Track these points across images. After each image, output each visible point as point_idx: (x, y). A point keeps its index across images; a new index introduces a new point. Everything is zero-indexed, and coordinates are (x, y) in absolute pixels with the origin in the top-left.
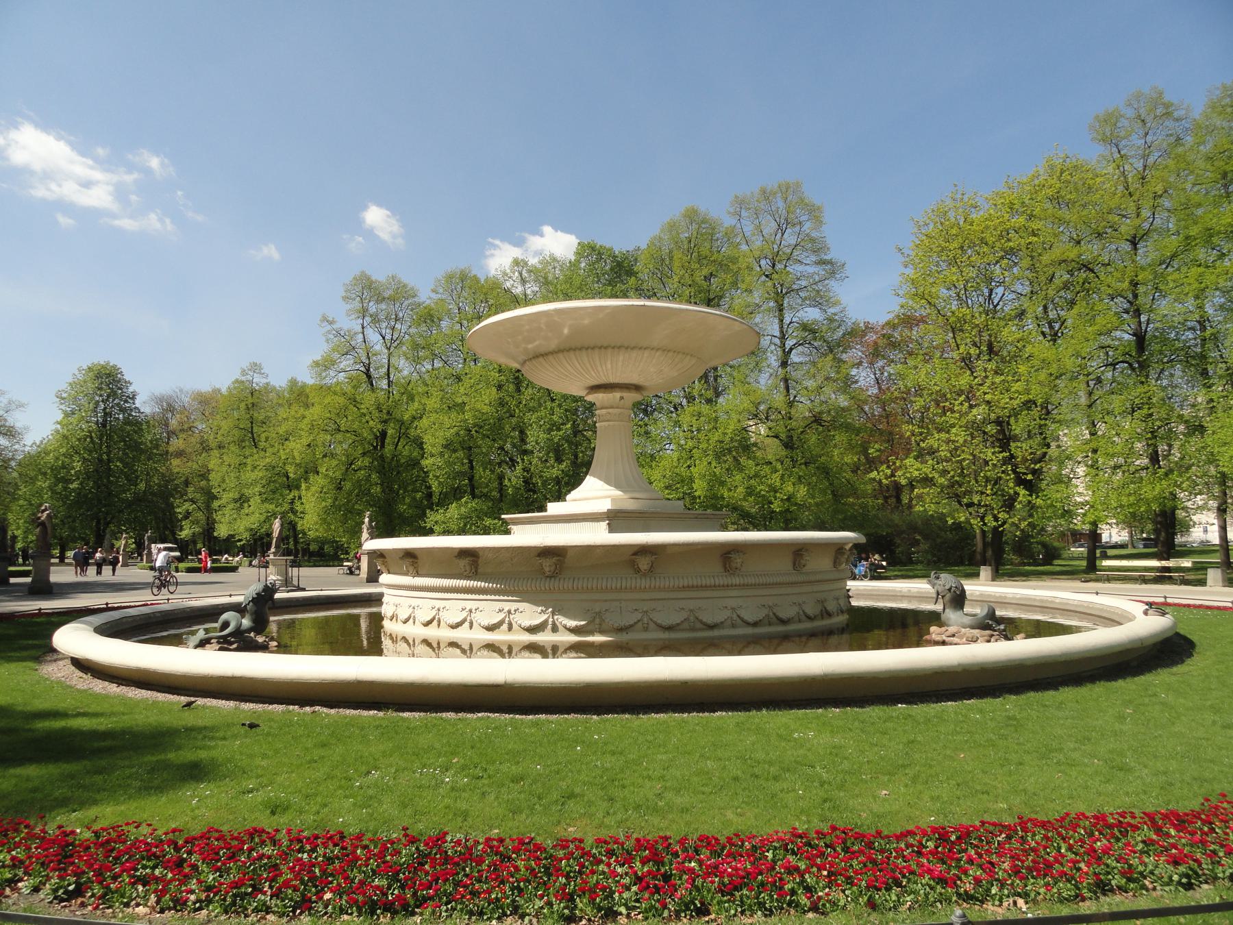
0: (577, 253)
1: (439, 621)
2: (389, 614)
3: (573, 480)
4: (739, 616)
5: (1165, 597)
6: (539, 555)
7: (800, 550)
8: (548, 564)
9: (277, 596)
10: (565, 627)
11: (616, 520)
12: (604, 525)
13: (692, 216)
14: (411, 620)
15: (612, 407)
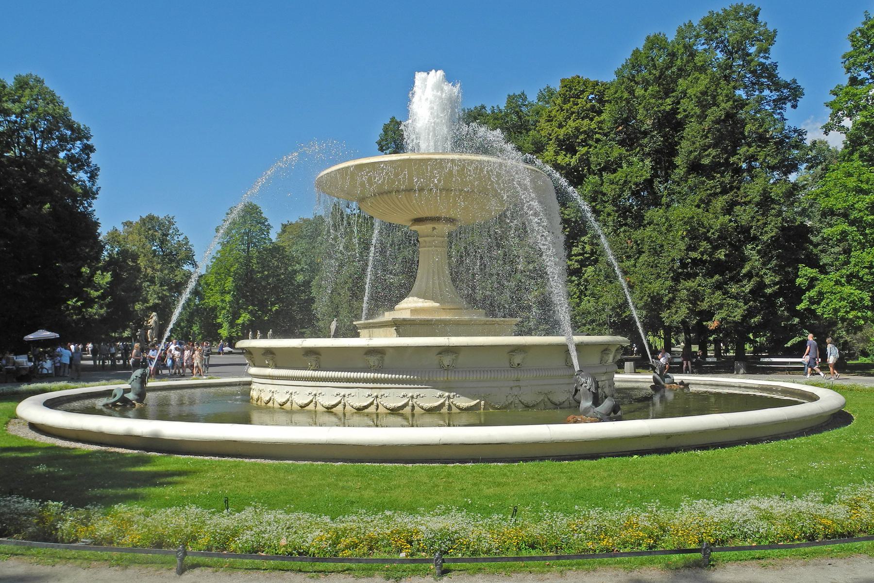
1: (378, 406)
4: (549, 399)
6: (440, 353)
8: (373, 360)
13: (648, 38)
15: (427, 236)
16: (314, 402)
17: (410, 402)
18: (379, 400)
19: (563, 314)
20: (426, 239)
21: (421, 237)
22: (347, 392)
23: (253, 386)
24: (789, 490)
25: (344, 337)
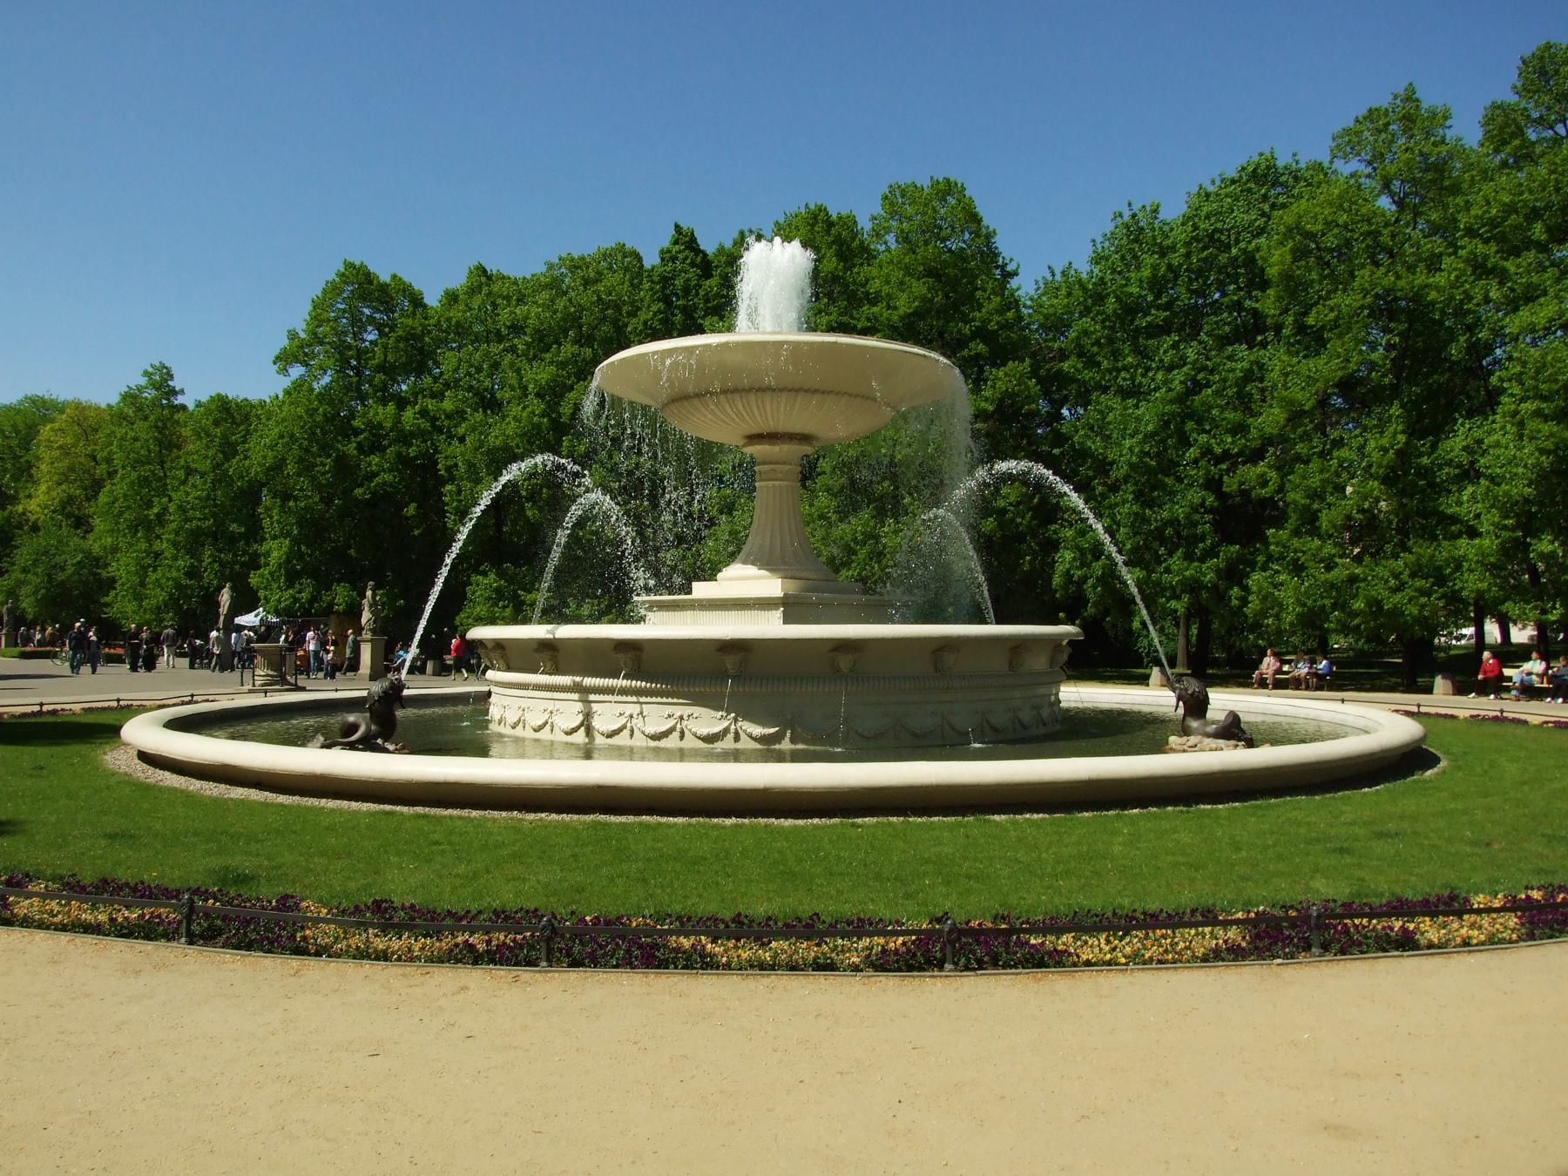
1: (632, 731)
2: (497, 717)
5: (1419, 706)
7: (1018, 647)
8: (730, 662)
9: (406, 692)
10: (750, 736)
12: (778, 614)
14: (521, 724)
17: (679, 726)
18: (684, 723)
20: (767, 467)
21: (759, 464)
23: (493, 699)
25: (576, 623)
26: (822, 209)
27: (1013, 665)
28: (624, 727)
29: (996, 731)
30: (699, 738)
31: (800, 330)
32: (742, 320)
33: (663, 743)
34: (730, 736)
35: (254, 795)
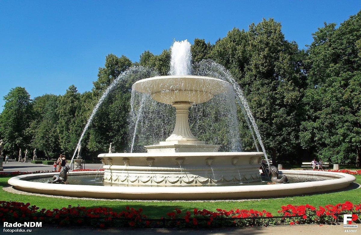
0: (286, 42)
3: (167, 134)
6: (176, 159)
8: (179, 162)
11: (178, 148)
12: (174, 149)
16: (127, 180)
18: (167, 179)
19: (235, 141)
22: (152, 175)
24: (138, 202)
26: (21, 88)
27: (250, 163)
28: (163, 180)
29: (247, 180)
30: (200, 182)
31: (189, 74)
32: (174, 74)
33: (147, 184)
34: (194, 182)
35: (26, 193)
